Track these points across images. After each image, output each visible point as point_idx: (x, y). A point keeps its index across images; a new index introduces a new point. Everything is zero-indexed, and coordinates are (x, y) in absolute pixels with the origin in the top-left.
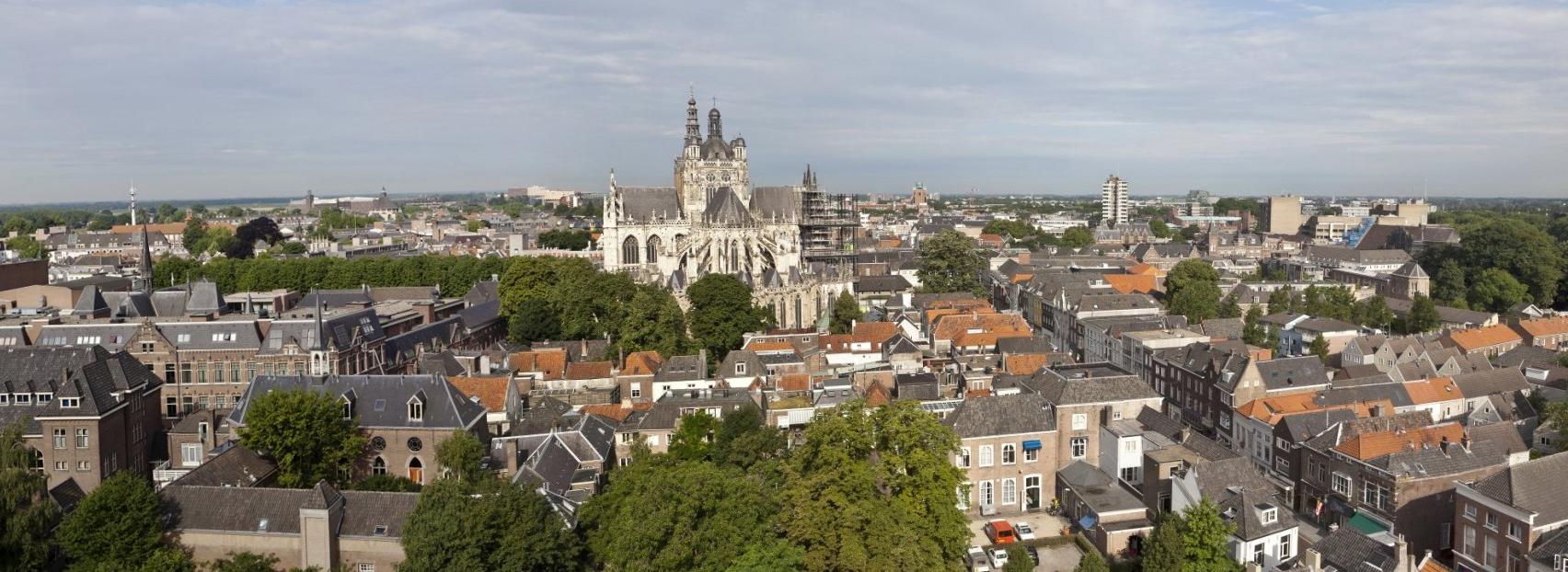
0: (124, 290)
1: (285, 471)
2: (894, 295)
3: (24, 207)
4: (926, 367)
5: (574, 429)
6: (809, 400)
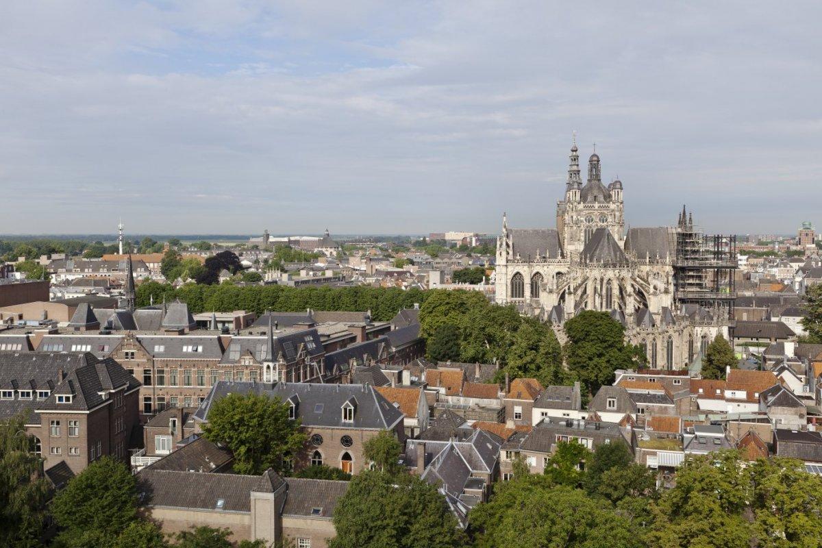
0: (112, 307)
1: (240, 460)
2: (774, 343)
3: (31, 237)
4: (810, 425)
5: (468, 441)
6: (680, 444)
